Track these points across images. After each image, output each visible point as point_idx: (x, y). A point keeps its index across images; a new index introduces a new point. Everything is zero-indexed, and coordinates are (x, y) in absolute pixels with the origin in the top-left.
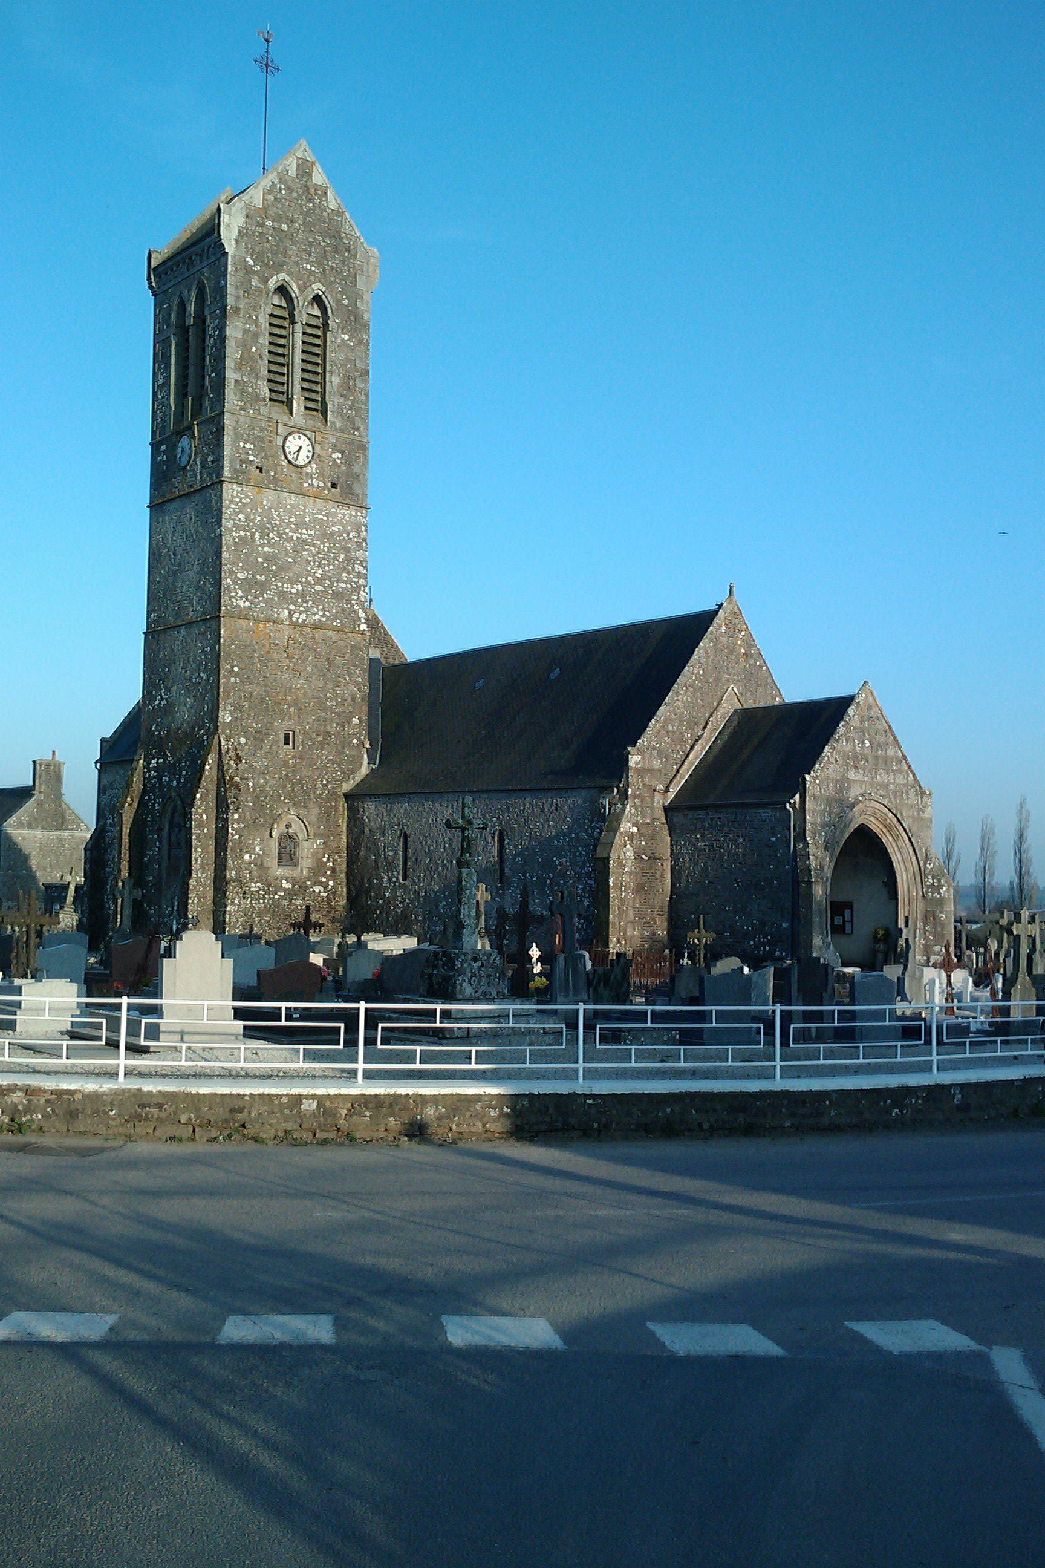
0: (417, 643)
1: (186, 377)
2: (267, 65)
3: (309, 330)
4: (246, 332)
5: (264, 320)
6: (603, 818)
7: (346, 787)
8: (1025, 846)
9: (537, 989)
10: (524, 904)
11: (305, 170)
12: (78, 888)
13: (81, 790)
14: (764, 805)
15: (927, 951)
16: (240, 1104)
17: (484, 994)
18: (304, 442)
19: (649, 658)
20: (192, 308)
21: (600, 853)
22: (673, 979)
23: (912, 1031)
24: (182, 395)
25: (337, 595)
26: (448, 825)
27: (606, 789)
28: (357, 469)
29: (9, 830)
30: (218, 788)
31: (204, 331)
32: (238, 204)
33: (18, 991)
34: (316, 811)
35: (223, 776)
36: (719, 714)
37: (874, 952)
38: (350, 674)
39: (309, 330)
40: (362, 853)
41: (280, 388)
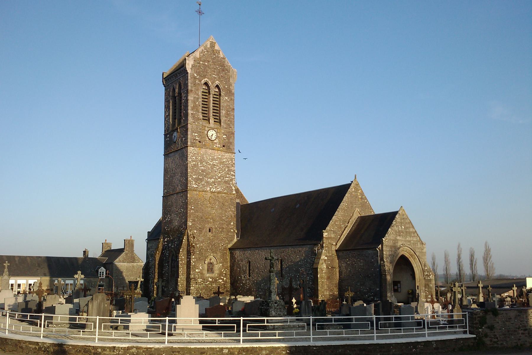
0: (252, 196)
1: (175, 112)
2: (200, 12)
3: (215, 96)
4: (194, 97)
5: (200, 94)
6: (315, 254)
7: (230, 246)
8: (460, 260)
9: (296, 313)
10: (291, 284)
11: (212, 45)
12: (141, 282)
13: (141, 250)
14: (368, 249)
15: (426, 297)
16: (204, 351)
17: (279, 314)
18: (214, 132)
19: (330, 200)
20: (177, 90)
21: (315, 266)
22: (340, 308)
23: (420, 324)
24: (174, 118)
25: (226, 182)
26: (266, 259)
27: (316, 245)
28: (231, 141)
29: (116, 263)
30: (187, 248)
31: (181, 98)
32: (191, 57)
33: (130, 316)
34: (220, 254)
35: (189, 243)
36: (353, 218)
37: (408, 298)
38: (230, 208)
39: (215, 96)
40: (235, 268)
41: (205, 115)
